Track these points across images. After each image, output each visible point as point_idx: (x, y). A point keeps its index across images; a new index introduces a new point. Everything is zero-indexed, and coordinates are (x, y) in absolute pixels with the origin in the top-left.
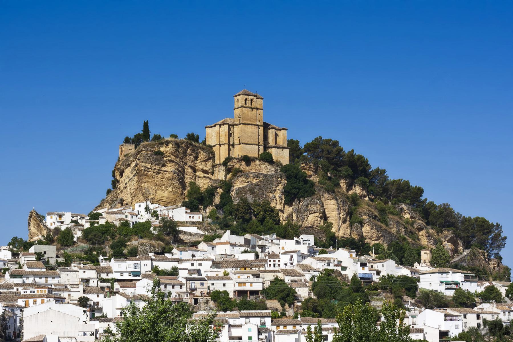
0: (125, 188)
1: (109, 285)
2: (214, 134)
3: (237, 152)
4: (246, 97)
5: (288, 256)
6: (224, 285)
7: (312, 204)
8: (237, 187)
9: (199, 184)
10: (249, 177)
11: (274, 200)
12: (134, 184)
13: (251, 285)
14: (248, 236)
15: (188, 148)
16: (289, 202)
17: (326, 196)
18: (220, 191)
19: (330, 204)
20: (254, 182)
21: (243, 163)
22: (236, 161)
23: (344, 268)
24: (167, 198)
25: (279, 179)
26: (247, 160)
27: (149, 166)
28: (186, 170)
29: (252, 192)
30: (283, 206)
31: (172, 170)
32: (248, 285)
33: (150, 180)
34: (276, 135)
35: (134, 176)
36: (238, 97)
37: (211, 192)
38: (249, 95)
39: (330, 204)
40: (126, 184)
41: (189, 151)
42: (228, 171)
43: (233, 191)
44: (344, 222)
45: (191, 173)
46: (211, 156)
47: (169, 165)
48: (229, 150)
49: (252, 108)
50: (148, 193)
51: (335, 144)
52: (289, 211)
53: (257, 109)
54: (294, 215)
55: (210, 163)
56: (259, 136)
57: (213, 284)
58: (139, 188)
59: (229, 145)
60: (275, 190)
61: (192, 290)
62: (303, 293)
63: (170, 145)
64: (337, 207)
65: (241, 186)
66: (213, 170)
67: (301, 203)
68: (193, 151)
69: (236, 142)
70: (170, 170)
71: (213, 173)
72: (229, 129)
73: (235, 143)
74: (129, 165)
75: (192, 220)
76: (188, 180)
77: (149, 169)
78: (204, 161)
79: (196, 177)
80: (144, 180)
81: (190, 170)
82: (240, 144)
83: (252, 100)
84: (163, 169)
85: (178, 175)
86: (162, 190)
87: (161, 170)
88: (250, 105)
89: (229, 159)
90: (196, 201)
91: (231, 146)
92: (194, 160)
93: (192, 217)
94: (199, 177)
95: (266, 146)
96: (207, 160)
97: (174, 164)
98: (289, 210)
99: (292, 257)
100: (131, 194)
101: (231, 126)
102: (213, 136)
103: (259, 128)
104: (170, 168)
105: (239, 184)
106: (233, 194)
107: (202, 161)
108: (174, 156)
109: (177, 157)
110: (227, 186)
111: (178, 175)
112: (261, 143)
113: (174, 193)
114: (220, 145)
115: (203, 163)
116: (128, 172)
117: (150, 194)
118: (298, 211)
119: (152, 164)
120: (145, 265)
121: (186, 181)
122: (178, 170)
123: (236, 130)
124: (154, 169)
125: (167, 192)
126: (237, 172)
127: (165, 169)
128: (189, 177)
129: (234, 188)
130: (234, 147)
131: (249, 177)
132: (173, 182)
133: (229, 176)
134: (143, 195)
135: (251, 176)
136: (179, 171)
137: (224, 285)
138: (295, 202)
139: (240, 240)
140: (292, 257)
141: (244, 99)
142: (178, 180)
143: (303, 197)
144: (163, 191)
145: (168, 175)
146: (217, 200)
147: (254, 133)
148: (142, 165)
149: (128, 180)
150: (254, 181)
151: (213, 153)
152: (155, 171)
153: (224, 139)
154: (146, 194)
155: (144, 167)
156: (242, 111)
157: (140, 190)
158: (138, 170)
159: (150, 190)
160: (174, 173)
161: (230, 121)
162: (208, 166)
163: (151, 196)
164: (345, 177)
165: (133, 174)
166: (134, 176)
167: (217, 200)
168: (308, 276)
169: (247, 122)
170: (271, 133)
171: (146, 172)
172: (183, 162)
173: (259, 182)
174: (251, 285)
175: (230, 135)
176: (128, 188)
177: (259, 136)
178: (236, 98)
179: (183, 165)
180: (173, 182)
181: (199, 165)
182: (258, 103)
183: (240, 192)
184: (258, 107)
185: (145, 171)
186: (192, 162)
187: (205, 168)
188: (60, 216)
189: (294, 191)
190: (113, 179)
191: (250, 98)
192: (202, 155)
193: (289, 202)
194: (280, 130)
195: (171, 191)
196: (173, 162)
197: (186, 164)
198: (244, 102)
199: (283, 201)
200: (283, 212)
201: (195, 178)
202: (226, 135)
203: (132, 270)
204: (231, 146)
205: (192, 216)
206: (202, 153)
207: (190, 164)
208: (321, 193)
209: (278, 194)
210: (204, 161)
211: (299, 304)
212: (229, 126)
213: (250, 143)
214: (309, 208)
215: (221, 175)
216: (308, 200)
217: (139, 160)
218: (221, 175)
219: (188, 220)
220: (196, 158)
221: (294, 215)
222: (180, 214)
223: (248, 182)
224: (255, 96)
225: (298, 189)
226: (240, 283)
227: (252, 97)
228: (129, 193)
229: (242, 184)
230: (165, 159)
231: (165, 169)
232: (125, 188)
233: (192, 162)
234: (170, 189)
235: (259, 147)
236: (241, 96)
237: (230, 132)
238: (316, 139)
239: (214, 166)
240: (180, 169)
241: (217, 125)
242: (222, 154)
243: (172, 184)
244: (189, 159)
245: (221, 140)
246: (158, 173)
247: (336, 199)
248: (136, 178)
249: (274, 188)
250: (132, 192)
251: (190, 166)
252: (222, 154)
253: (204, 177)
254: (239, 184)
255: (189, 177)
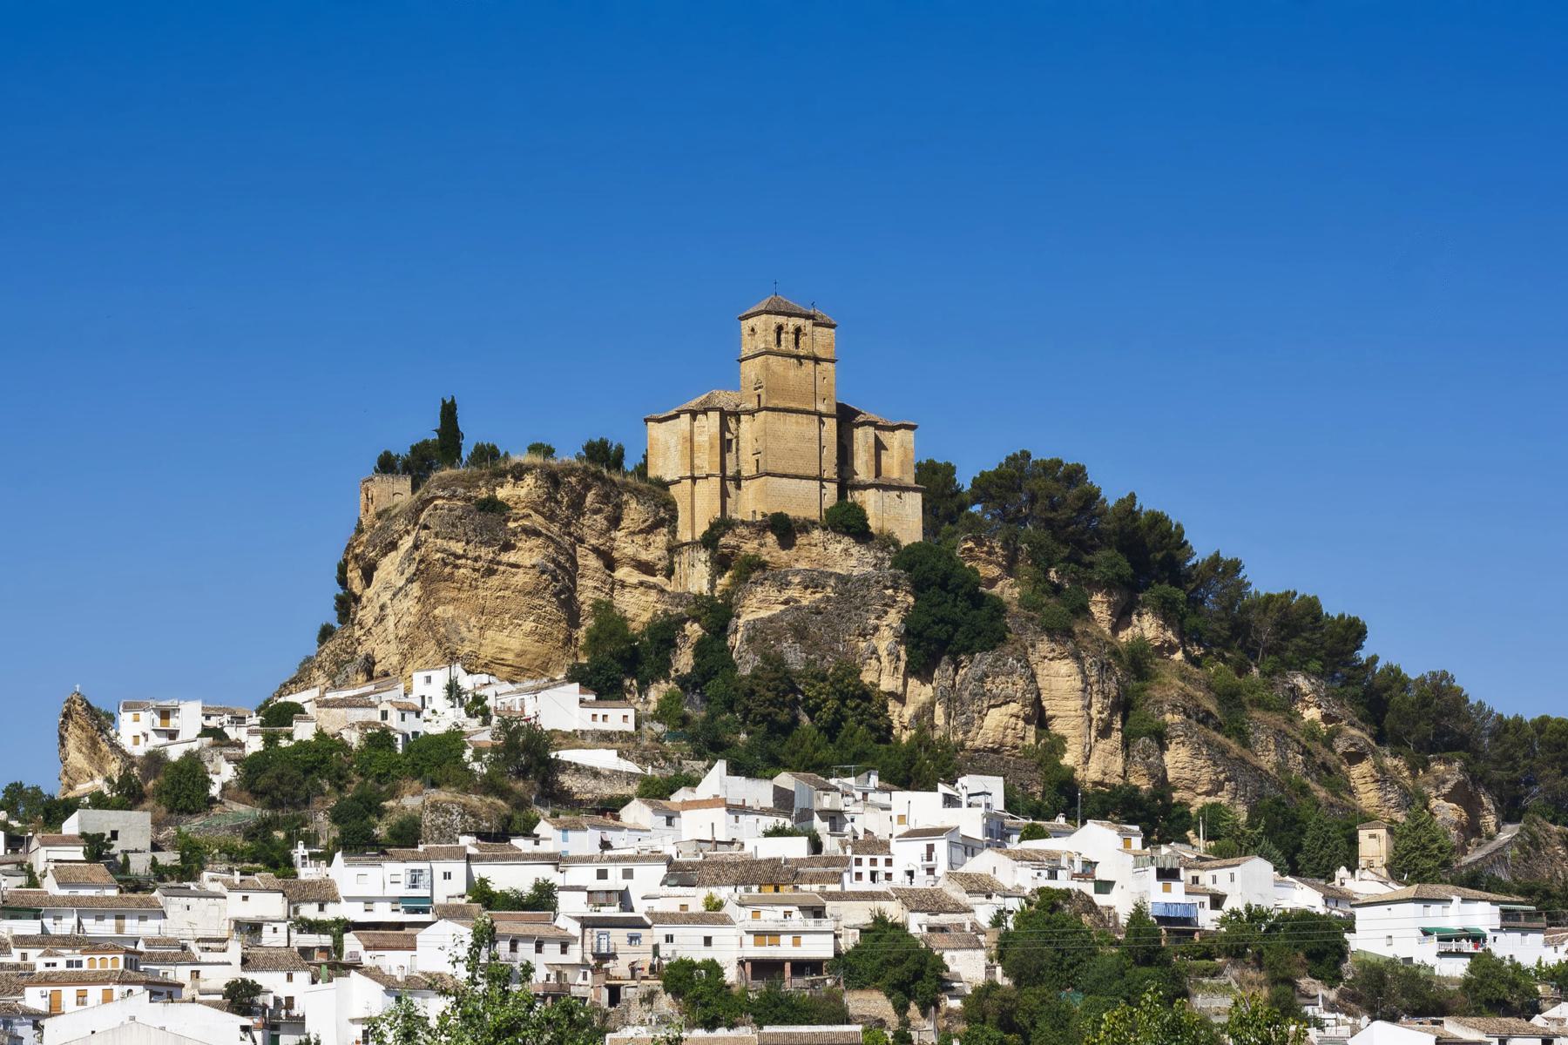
0: (380, 620)
1: (327, 940)
2: (673, 442)
3: (751, 502)
4: (781, 319)
5: (920, 846)
6: (708, 941)
7: (997, 675)
8: (751, 617)
9: (623, 607)
10: (789, 584)
11: (873, 662)
12: (408, 607)
13: (796, 943)
14: (785, 780)
15: (588, 488)
16: (920, 668)
17: (1044, 646)
18: (694, 630)
19: (1057, 675)
20: (805, 603)
21: (771, 538)
22: (745, 532)
23: (1104, 887)
24: (518, 655)
25: (890, 592)
26: (784, 529)
27: (458, 548)
28: (580, 561)
29: (800, 634)
30: (900, 682)
31: (534, 561)
32: (786, 940)
33: (463, 595)
34: (879, 446)
35: (410, 581)
36: (751, 322)
37: (664, 635)
38: (790, 315)
39: (1057, 675)
40: (382, 608)
41: (590, 497)
42: (721, 563)
43: (736, 631)
44: (1104, 732)
45: (596, 570)
46: (665, 515)
47: (526, 544)
48: (724, 494)
49: (799, 358)
50: (455, 638)
51: (1075, 475)
52: (922, 698)
53: (817, 360)
54: (939, 711)
55: (660, 539)
56: (821, 448)
57: (669, 939)
58: (427, 623)
59: (724, 478)
60: (876, 629)
61: (602, 958)
62: (969, 967)
63: (529, 480)
64: (1079, 685)
65: (764, 614)
66: (672, 563)
67: (962, 672)
68: (605, 498)
69: (748, 469)
70: (528, 563)
71: (670, 572)
72: (724, 427)
73: (744, 474)
74: (393, 546)
75: (600, 725)
76: (587, 594)
77: (458, 557)
78: (641, 531)
79: (613, 583)
80: (443, 594)
81: (593, 562)
82: (759, 475)
83: (798, 331)
84: (504, 557)
85: (555, 579)
86: (502, 628)
87: (499, 563)
88: (791, 347)
89: (723, 525)
90: (613, 665)
91: (730, 481)
92: (609, 530)
93: (600, 718)
94: (623, 585)
95: (846, 483)
96: (650, 530)
97: (540, 541)
98: (920, 692)
99: (930, 848)
100: (400, 640)
101: (729, 416)
102: (669, 449)
103: (821, 422)
104: (529, 554)
105: (758, 606)
106: (736, 640)
107: (633, 533)
108: (542, 514)
109: (551, 518)
110: (717, 615)
111: (555, 579)
112: (830, 471)
113: (542, 638)
114: (694, 479)
115: (639, 539)
116: (390, 569)
117: (463, 640)
118: (951, 698)
119: (468, 543)
120: (447, 876)
121: (581, 599)
122: (554, 561)
123: (747, 429)
124: (476, 560)
125: (518, 633)
126: (750, 571)
127: (511, 557)
128: (591, 583)
129: (741, 621)
130: (738, 487)
131: (789, 584)
132: (537, 602)
133: (724, 581)
134: (439, 644)
135: (797, 580)
136: (558, 565)
137: (708, 941)
138: (943, 666)
139: (759, 792)
140: (930, 848)
141: (774, 327)
142: (556, 595)
143: (969, 651)
144: (506, 632)
145: (520, 579)
146: (684, 661)
147: (806, 439)
148: (436, 546)
149: (389, 594)
150: (808, 599)
151: (671, 506)
152: (477, 565)
153: (707, 461)
154: (449, 640)
155: (444, 551)
156: (767, 367)
157: (430, 628)
158: (421, 561)
159: (463, 629)
160: (543, 572)
161: (725, 399)
162: (655, 551)
163: (466, 649)
164: (1108, 586)
165: (407, 575)
166: (410, 581)
167: (684, 661)
168: (984, 913)
169: (781, 405)
170: (862, 438)
171: (448, 570)
172: (570, 534)
173: (821, 600)
174: (796, 943)
175: (725, 446)
176: (390, 621)
177: (821, 448)
178: (746, 325)
179: (573, 545)
180: (537, 602)
181: (625, 545)
182: (821, 340)
183: (757, 633)
184: (820, 353)
185: (446, 564)
186: (602, 534)
187: (644, 556)
188: (165, 714)
189: (941, 631)
190: (341, 592)
191: (791, 323)
192: (635, 513)
193: (920, 668)
194: (893, 429)
195: (532, 633)
196: (538, 534)
197: (581, 541)
198: (772, 337)
199: (902, 665)
200: (901, 699)
201: (612, 590)
202: (712, 446)
203: (402, 890)
204: (730, 481)
205: (600, 712)
206: (633, 504)
207: (593, 542)
208: (1028, 637)
209: (884, 641)
210: (641, 531)
211: (956, 1004)
212: (724, 415)
213: (792, 471)
214: (988, 686)
215: (696, 577)
216: (984, 661)
217: (426, 527)
218: (696, 577)
219: (589, 725)
220: (615, 522)
221: (939, 711)
222: (560, 708)
223: (786, 602)
224: (808, 317)
225: (950, 624)
226: (759, 934)
227: (800, 322)
228: (391, 637)
229: (767, 608)
230: (511, 525)
231: (512, 560)
232: (380, 620)
233: (602, 534)
234: (529, 625)
235: (822, 487)
236: (764, 317)
237: (728, 436)
238: (1012, 460)
239: (673, 549)
240: (562, 559)
241: (685, 412)
242: (698, 508)
243: (534, 607)
244: (591, 524)
245: (696, 461)
246: (490, 572)
247: (1077, 658)
248: (415, 589)
249: (873, 621)
250: (402, 633)
251: (595, 550)
252: (698, 508)
253: (641, 583)
254: (758, 606)
255: (591, 583)
